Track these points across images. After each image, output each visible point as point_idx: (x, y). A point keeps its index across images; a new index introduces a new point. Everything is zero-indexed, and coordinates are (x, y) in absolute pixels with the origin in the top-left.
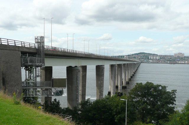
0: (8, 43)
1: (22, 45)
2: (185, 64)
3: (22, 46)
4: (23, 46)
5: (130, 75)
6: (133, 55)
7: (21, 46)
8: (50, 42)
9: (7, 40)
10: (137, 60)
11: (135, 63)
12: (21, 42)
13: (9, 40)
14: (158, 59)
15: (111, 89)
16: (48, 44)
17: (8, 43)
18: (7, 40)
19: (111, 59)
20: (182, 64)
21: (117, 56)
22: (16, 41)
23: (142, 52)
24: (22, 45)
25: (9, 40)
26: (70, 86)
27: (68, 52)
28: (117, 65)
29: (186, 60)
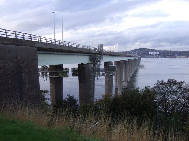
0: (6, 35)
1: (38, 40)
2: (183, 58)
3: (77, 47)
4: (40, 41)
5: (125, 80)
6: (133, 50)
7: (37, 41)
8: (53, 34)
9: (22, 34)
10: (137, 55)
11: (137, 58)
12: (14, 33)
13: (17, 33)
14: (158, 55)
15: (118, 86)
16: (105, 48)
17: (6, 35)
18: (14, 33)
19: (119, 55)
20: (181, 58)
21: (125, 52)
22: (47, 39)
23: (143, 48)
24: (38, 40)
25: (69, 43)
26: (82, 85)
27: (55, 45)
28: (123, 61)
29: (184, 55)
